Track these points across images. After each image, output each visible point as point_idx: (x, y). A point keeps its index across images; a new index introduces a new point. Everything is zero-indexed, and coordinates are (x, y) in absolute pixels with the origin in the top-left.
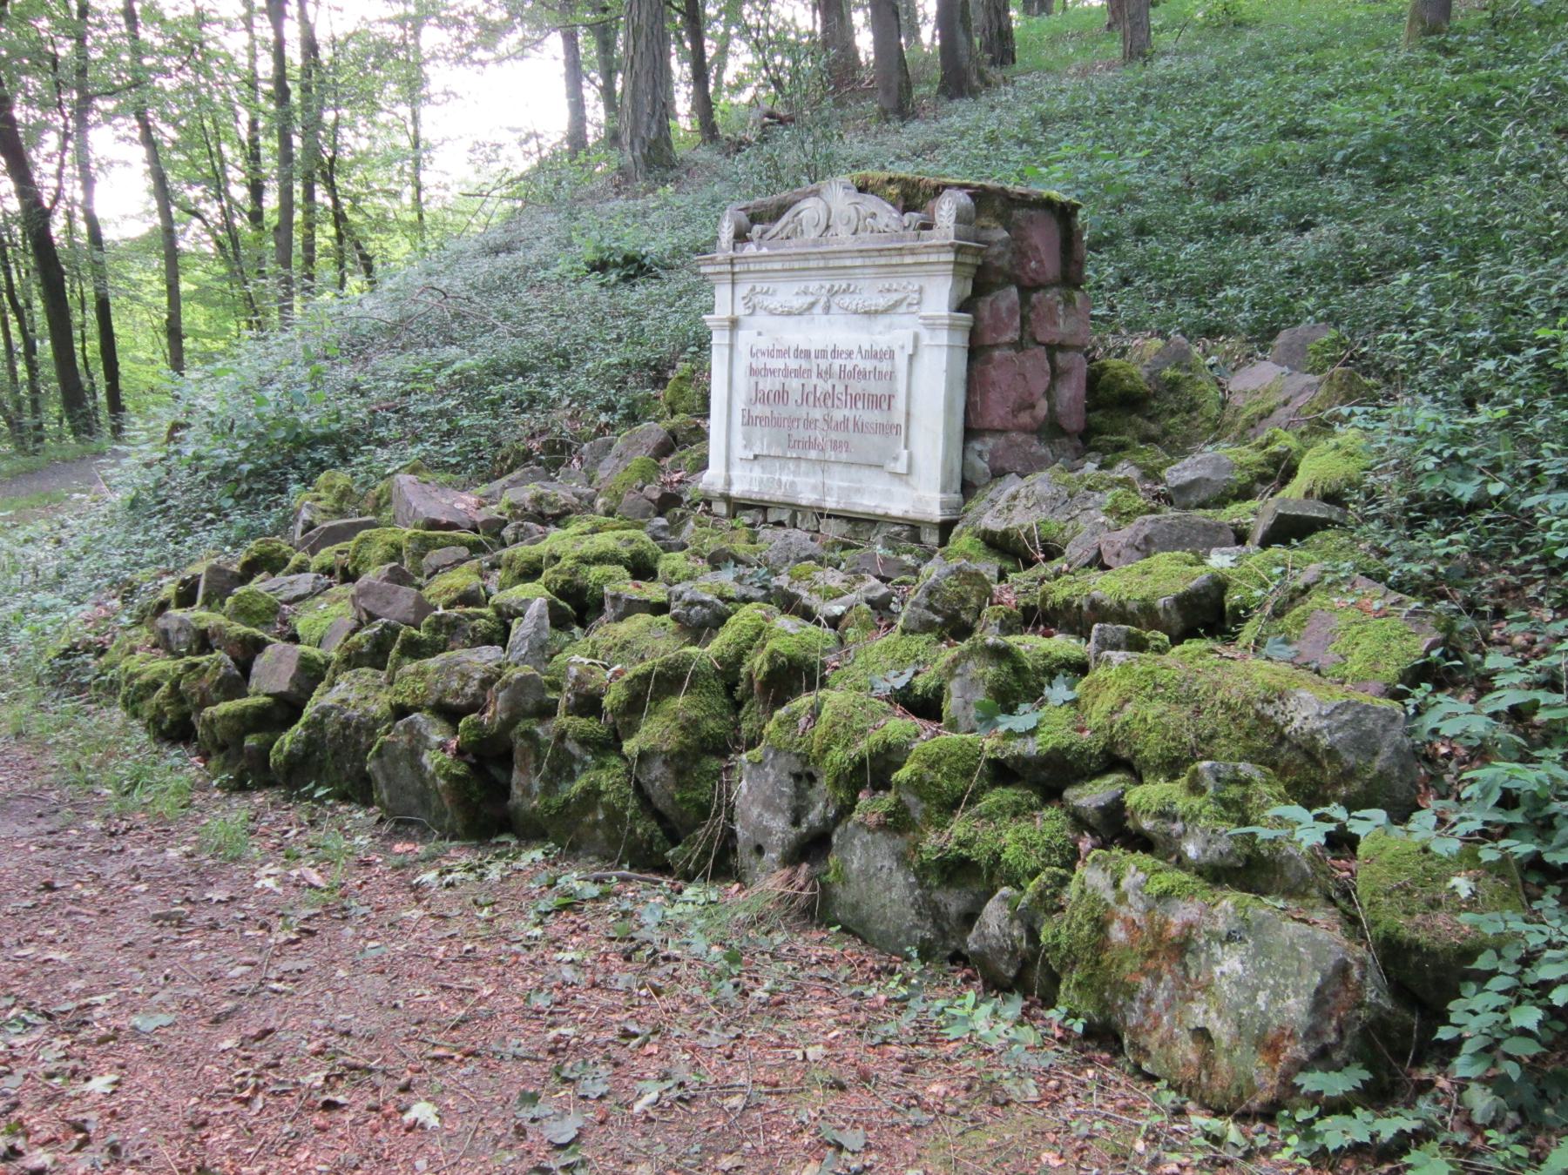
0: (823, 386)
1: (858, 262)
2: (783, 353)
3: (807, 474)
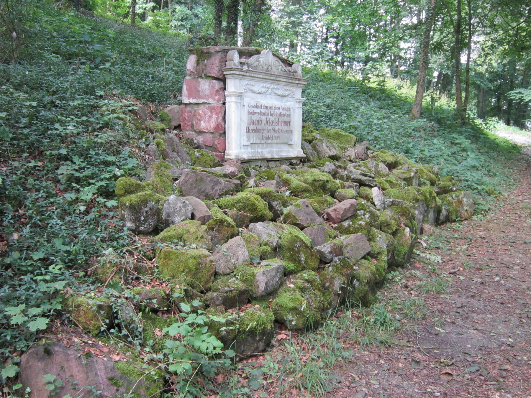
0: (272, 119)
3: (266, 148)
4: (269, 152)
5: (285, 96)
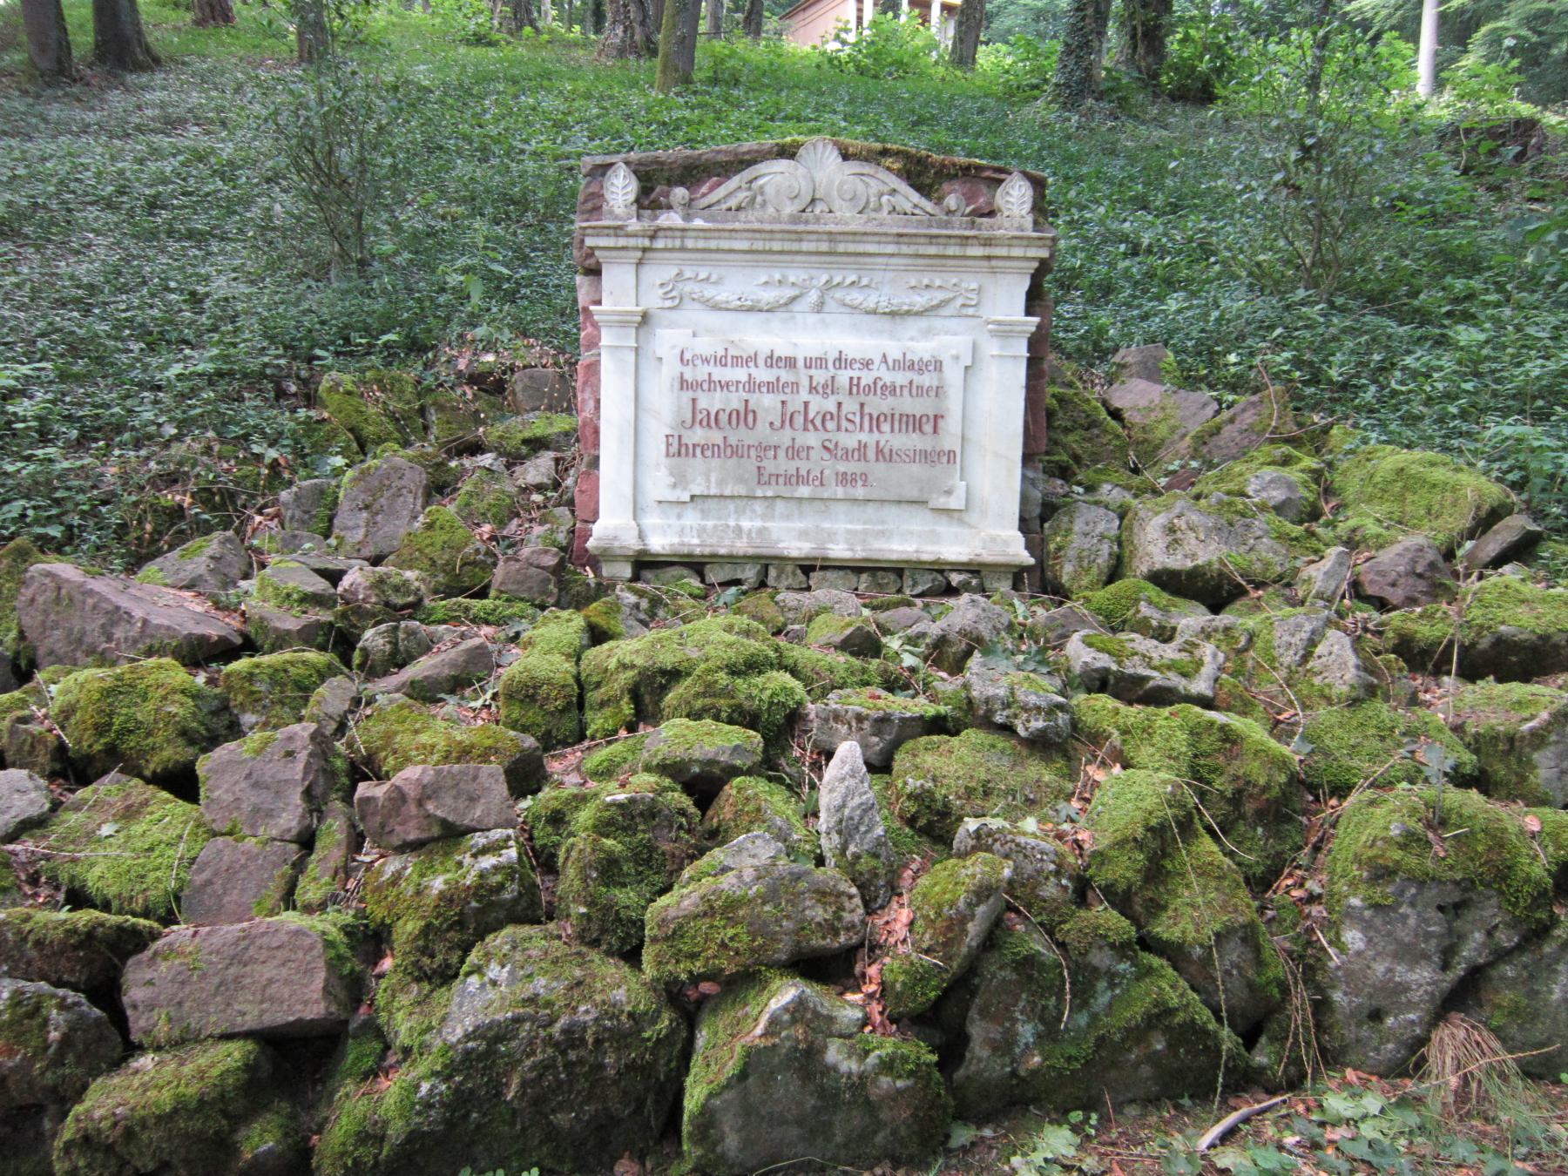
0: (818, 404)
1: (890, 249)
2: (738, 361)
3: (788, 517)
4: (803, 535)
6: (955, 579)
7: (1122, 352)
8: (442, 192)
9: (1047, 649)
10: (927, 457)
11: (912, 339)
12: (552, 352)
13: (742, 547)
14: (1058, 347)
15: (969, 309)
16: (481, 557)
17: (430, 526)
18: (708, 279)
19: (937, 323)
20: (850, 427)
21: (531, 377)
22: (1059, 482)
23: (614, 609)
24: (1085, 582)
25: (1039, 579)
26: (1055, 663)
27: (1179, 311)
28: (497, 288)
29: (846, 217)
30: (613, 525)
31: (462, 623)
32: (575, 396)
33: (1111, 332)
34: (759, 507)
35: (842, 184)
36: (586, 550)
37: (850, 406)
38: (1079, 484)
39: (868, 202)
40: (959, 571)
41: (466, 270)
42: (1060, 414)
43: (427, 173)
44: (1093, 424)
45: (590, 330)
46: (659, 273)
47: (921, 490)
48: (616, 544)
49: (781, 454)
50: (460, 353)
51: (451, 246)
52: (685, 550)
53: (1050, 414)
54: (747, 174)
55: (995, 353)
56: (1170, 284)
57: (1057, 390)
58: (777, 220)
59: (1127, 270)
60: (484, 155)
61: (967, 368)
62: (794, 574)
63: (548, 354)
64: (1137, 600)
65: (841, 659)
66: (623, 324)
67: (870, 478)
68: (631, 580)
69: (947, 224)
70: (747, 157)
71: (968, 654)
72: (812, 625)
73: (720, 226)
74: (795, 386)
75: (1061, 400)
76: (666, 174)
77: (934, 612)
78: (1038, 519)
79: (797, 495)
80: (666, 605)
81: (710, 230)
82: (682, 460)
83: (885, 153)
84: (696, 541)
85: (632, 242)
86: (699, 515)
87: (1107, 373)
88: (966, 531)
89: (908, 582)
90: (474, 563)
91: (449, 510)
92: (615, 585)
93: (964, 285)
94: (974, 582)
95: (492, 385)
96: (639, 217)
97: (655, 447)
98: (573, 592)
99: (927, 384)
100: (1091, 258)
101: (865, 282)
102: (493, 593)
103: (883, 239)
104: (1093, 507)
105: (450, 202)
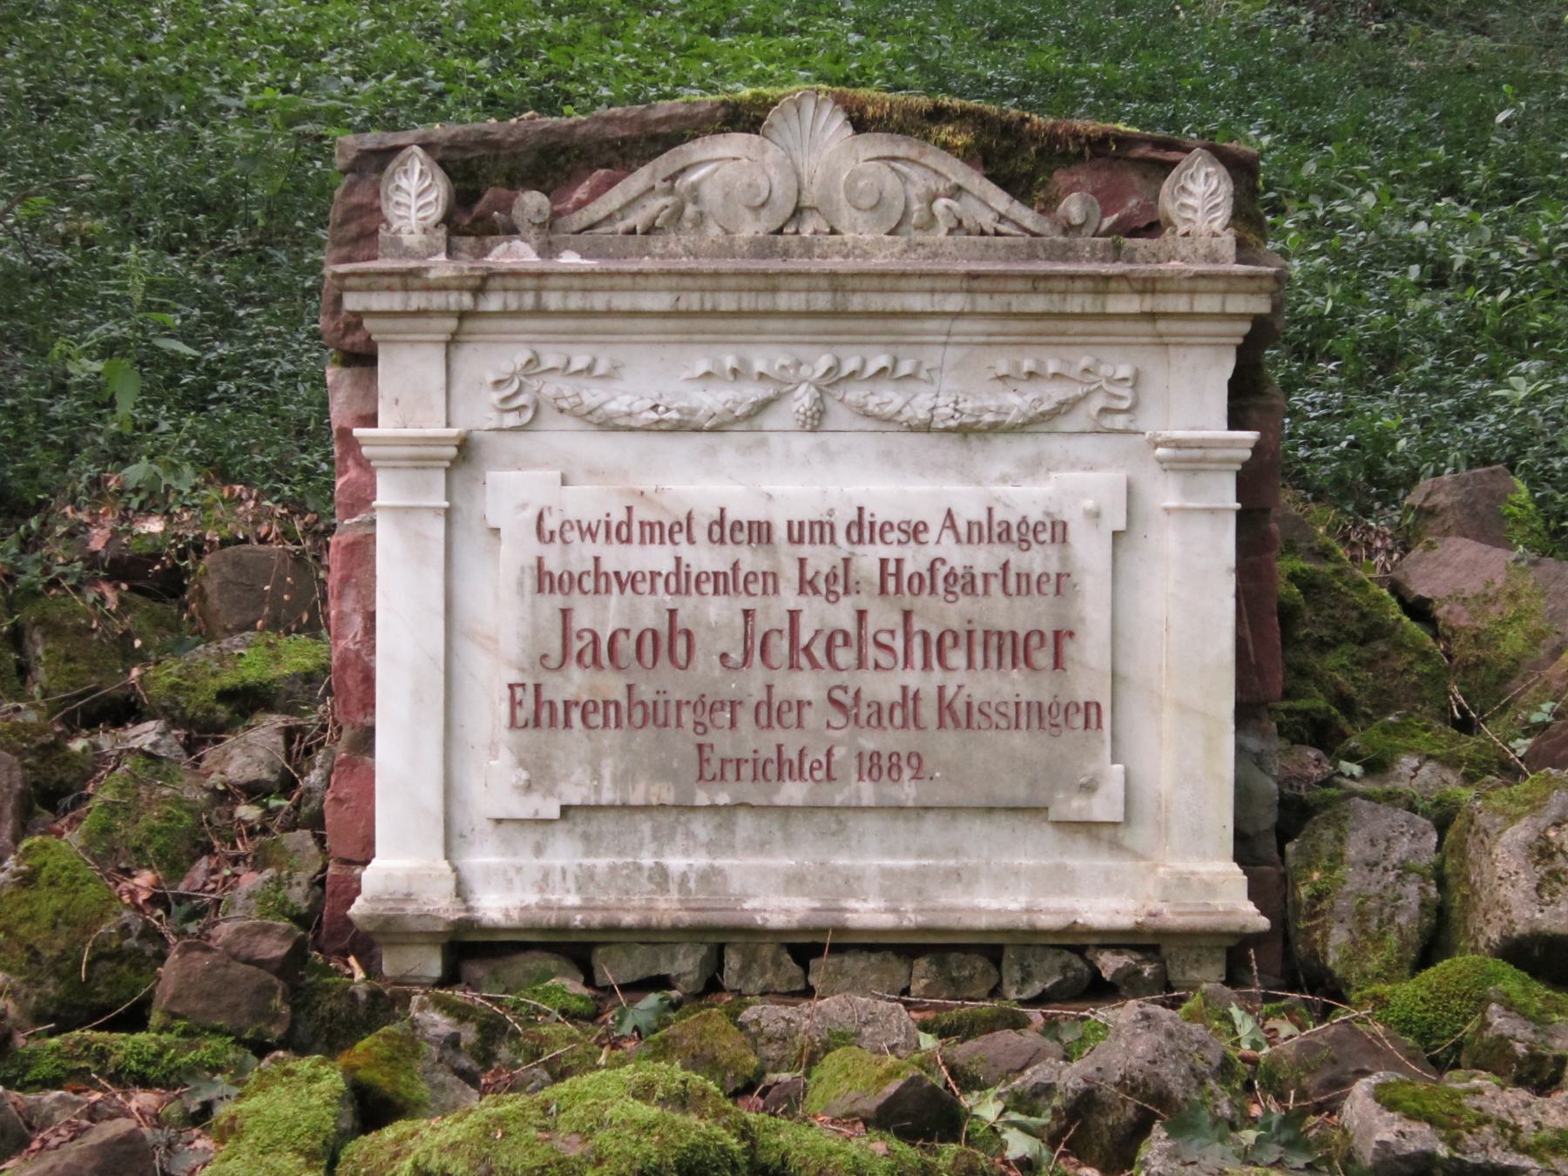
0: (817, 615)
1: (954, 303)
3: (762, 847)
4: (795, 881)
5: (995, 428)
6: (1110, 964)
7: (1425, 484)
8: (64, 189)
9: (1302, 1113)
10: (1041, 716)
11: (1004, 479)
12: (279, 510)
13: (668, 909)
14: (1299, 479)
15: (1115, 419)
16: (132, 942)
17: (27, 880)
18: (589, 369)
19: (1054, 446)
20: (885, 659)
21: (237, 563)
22: (1312, 753)
23: (408, 1047)
24: (1374, 964)
25: (1279, 960)
26: (1323, 1142)
27: (1534, 399)
28: (162, 375)
29: (865, 242)
30: (402, 867)
31: (93, 1085)
32: (325, 600)
33: (1402, 443)
34: (701, 827)
35: (854, 177)
36: (349, 922)
37: (883, 617)
38: (1352, 757)
39: (906, 213)
40: (1117, 948)
41: (108, 349)
42: (1308, 614)
43: (37, 153)
44: (1375, 631)
45: (353, 473)
46: (491, 360)
47: (1033, 784)
48: (411, 909)
49: (745, 717)
50: (95, 517)
51: (80, 298)
52: (552, 918)
53: (1288, 615)
54: (665, 163)
55: (1172, 502)
56: (1513, 342)
57: (1299, 564)
58: (728, 251)
59: (1425, 316)
60: (148, 114)
61: (1115, 534)
62: (777, 963)
63: (270, 515)
64: (1483, 1002)
65: (878, 1147)
66: (420, 463)
67: (928, 764)
68: (442, 983)
69: (1065, 254)
70: (663, 129)
71: (1140, 1129)
72: (816, 1074)
73: (613, 265)
74: (771, 581)
75: (1308, 584)
76: (505, 166)
77: (1067, 1037)
78: (1272, 833)
79: (780, 800)
80: (515, 1035)
81: (592, 274)
82: (542, 734)
83: (938, 115)
84: (573, 900)
85: (437, 300)
86: (579, 846)
87: (1397, 527)
88: (1127, 865)
89: (1012, 973)
90: (119, 956)
91: (69, 842)
92: (408, 997)
93: (1105, 370)
94: (1147, 970)
95: (158, 580)
96: (450, 253)
97: (487, 711)
98: (323, 1011)
99: (1037, 570)
100: (1354, 294)
101: (905, 368)
102: (155, 1019)
103: (940, 284)
104: (1383, 809)
105: (79, 208)
